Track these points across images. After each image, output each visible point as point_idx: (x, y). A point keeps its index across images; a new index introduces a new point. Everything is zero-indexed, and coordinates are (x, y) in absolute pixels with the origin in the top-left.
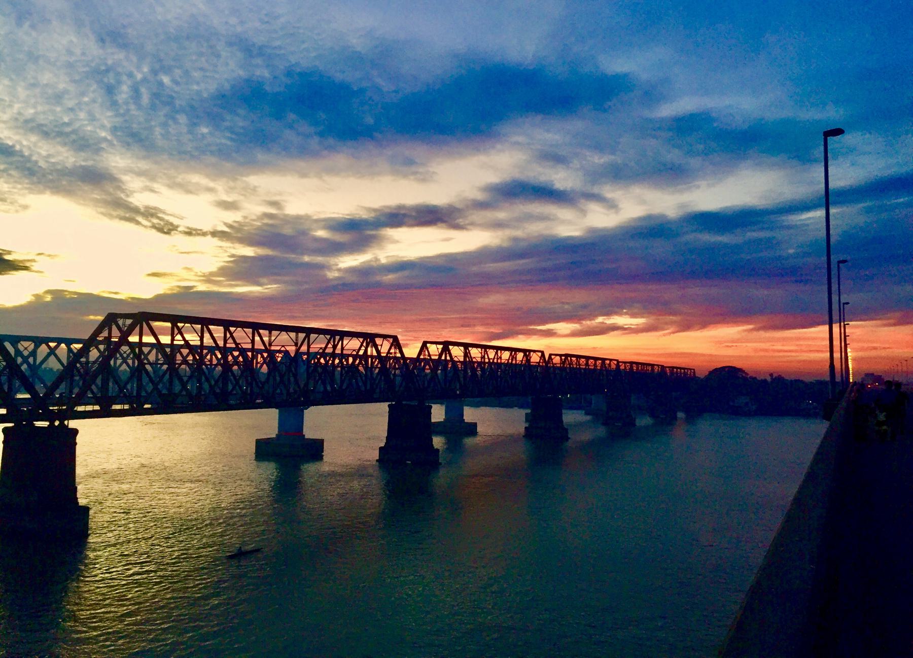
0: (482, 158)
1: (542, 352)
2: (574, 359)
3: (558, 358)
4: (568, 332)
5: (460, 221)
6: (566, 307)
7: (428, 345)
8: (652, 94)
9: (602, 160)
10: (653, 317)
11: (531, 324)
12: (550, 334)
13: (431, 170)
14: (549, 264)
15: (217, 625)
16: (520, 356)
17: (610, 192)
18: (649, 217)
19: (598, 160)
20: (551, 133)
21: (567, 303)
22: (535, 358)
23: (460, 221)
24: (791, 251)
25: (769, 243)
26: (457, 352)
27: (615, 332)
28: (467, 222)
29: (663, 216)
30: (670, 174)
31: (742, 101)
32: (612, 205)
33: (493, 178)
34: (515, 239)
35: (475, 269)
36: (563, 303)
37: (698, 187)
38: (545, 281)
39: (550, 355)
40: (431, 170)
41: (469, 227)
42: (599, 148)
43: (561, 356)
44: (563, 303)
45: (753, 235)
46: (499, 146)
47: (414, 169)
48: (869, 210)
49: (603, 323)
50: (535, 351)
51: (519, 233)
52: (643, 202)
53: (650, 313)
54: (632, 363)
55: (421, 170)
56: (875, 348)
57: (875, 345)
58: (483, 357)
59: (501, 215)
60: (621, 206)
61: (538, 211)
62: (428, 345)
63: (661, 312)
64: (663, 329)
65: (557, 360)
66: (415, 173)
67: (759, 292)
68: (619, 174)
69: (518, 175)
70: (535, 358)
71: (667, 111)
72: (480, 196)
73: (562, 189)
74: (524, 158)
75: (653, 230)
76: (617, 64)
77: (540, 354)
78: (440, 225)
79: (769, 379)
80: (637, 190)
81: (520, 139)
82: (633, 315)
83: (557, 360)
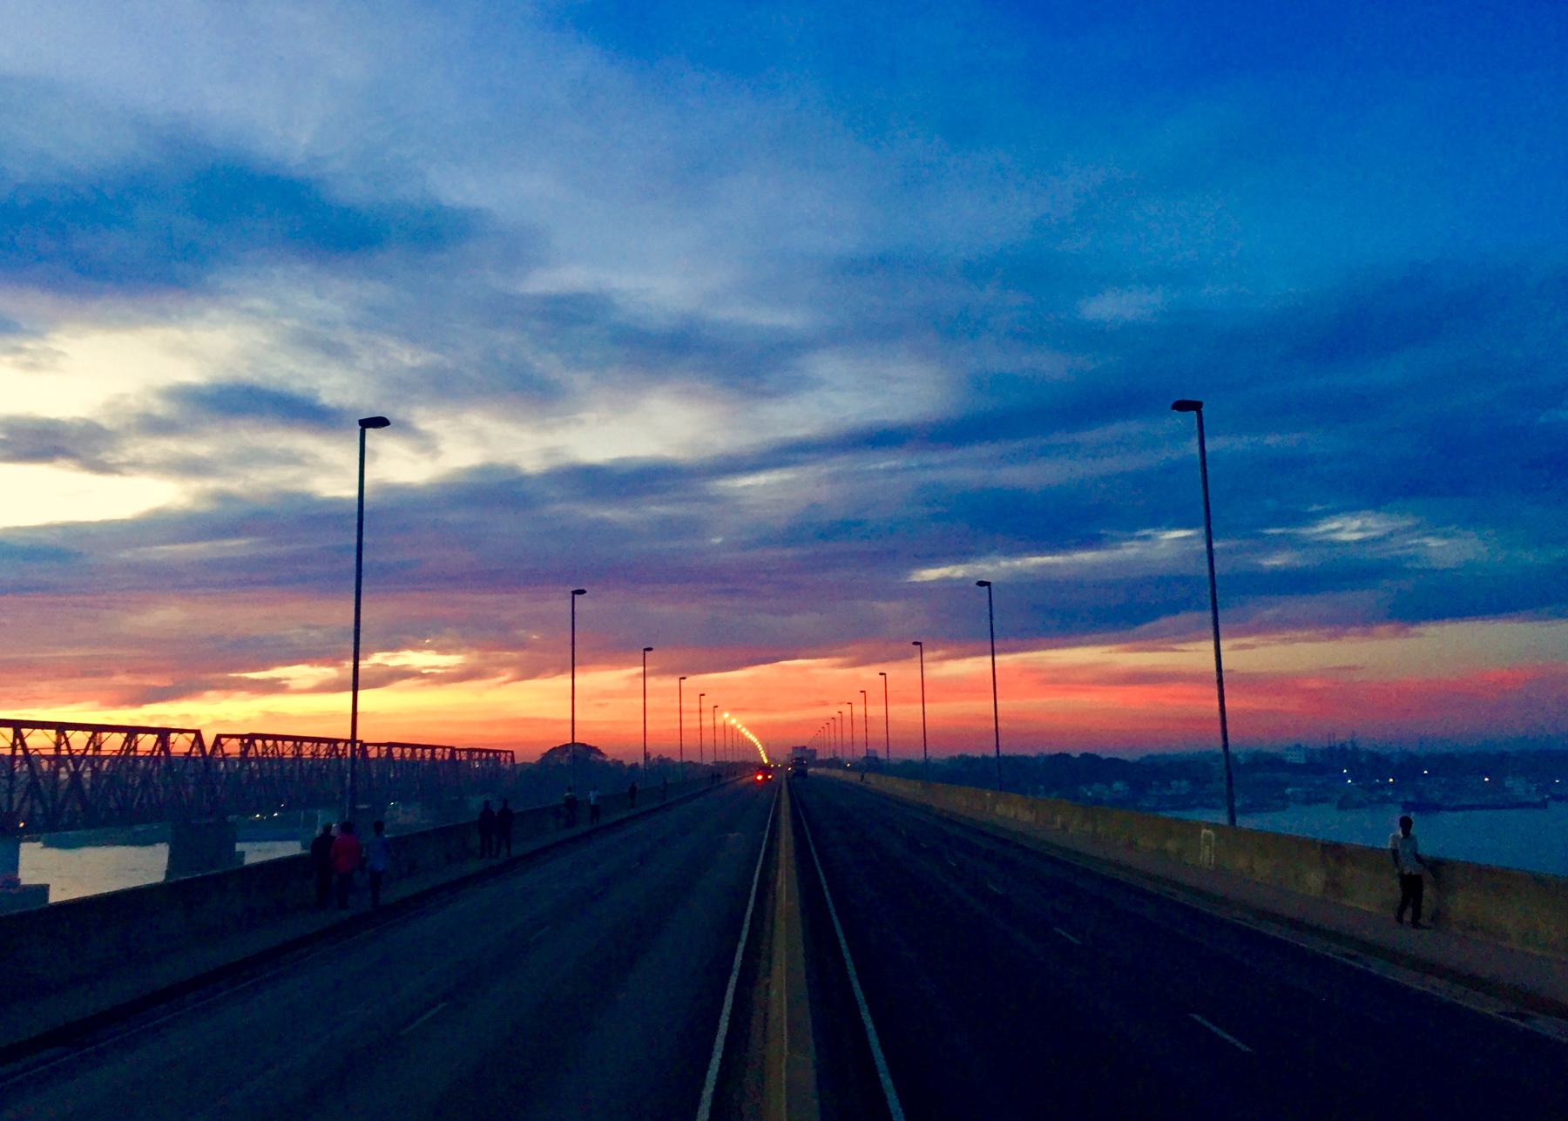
0: (174, 334)
1: (198, 733)
2: (269, 743)
3: (236, 742)
4: (310, 683)
5: (108, 456)
6: (313, 633)
7: (223, 740)
8: (519, 246)
9: (418, 361)
10: (476, 653)
11: (231, 671)
12: (275, 687)
13: (52, 345)
14: (284, 550)
15: (1359, 530)
16: (428, 751)
17: (427, 420)
18: (485, 470)
19: (408, 358)
20: (326, 297)
21: (317, 627)
22: (180, 744)
23: (108, 456)
24: (717, 540)
25: (692, 528)
26: (40, 741)
27: (405, 683)
28: (122, 459)
29: (512, 469)
30: (530, 393)
31: (659, 277)
32: (426, 444)
33: (190, 374)
34: (224, 498)
35: (126, 555)
36: (309, 627)
37: (581, 422)
38: (276, 582)
39: (219, 737)
40: (52, 345)
41: (126, 470)
42: (411, 337)
43: (241, 737)
44: (309, 627)
45: (656, 509)
46: (214, 313)
47: (14, 342)
48: (835, 478)
49: (379, 665)
50: (181, 731)
51: (235, 486)
52: (480, 437)
53: (472, 646)
54: (390, 745)
55: (29, 345)
56: (76, 605)
57: (824, 698)
58: (58, 747)
59: (200, 448)
60: (443, 447)
61: (280, 445)
62: (223, 740)
63: (497, 645)
64: (494, 675)
65: (233, 747)
66: (18, 350)
67: (661, 610)
68: (447, 388)
69: (245, 373)
70: (180, 744)
71: (541, 282)
72: (160, 408)
73: (333, 405)
74: (264, 341)
75: (495, 492)
76: (460, 187)
77: (192, 736)
78: (62, 462)
79: (641, 761)
80: (475, 419)
81: (259, 303)
82: (443, 650)
83: (233, 747)
